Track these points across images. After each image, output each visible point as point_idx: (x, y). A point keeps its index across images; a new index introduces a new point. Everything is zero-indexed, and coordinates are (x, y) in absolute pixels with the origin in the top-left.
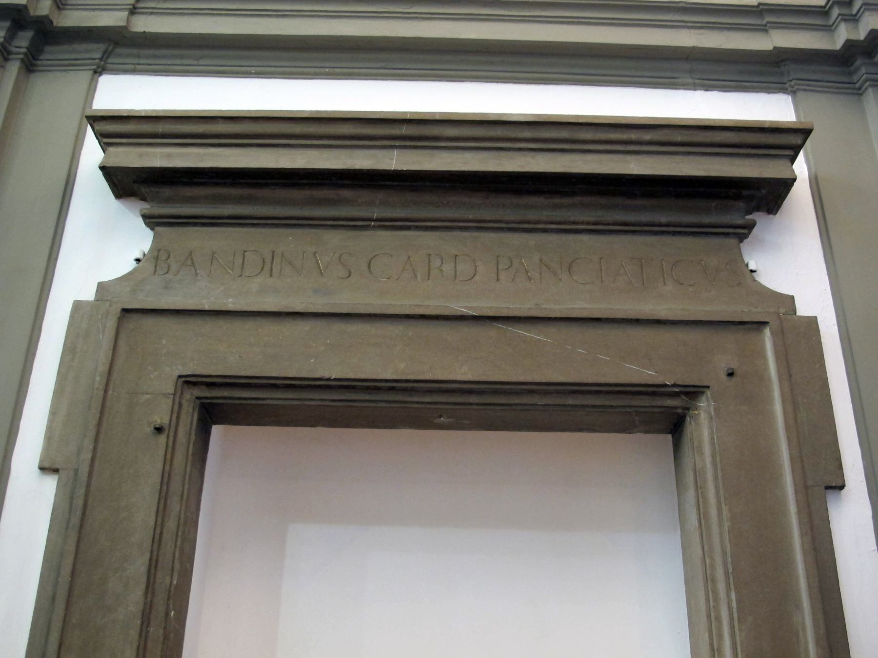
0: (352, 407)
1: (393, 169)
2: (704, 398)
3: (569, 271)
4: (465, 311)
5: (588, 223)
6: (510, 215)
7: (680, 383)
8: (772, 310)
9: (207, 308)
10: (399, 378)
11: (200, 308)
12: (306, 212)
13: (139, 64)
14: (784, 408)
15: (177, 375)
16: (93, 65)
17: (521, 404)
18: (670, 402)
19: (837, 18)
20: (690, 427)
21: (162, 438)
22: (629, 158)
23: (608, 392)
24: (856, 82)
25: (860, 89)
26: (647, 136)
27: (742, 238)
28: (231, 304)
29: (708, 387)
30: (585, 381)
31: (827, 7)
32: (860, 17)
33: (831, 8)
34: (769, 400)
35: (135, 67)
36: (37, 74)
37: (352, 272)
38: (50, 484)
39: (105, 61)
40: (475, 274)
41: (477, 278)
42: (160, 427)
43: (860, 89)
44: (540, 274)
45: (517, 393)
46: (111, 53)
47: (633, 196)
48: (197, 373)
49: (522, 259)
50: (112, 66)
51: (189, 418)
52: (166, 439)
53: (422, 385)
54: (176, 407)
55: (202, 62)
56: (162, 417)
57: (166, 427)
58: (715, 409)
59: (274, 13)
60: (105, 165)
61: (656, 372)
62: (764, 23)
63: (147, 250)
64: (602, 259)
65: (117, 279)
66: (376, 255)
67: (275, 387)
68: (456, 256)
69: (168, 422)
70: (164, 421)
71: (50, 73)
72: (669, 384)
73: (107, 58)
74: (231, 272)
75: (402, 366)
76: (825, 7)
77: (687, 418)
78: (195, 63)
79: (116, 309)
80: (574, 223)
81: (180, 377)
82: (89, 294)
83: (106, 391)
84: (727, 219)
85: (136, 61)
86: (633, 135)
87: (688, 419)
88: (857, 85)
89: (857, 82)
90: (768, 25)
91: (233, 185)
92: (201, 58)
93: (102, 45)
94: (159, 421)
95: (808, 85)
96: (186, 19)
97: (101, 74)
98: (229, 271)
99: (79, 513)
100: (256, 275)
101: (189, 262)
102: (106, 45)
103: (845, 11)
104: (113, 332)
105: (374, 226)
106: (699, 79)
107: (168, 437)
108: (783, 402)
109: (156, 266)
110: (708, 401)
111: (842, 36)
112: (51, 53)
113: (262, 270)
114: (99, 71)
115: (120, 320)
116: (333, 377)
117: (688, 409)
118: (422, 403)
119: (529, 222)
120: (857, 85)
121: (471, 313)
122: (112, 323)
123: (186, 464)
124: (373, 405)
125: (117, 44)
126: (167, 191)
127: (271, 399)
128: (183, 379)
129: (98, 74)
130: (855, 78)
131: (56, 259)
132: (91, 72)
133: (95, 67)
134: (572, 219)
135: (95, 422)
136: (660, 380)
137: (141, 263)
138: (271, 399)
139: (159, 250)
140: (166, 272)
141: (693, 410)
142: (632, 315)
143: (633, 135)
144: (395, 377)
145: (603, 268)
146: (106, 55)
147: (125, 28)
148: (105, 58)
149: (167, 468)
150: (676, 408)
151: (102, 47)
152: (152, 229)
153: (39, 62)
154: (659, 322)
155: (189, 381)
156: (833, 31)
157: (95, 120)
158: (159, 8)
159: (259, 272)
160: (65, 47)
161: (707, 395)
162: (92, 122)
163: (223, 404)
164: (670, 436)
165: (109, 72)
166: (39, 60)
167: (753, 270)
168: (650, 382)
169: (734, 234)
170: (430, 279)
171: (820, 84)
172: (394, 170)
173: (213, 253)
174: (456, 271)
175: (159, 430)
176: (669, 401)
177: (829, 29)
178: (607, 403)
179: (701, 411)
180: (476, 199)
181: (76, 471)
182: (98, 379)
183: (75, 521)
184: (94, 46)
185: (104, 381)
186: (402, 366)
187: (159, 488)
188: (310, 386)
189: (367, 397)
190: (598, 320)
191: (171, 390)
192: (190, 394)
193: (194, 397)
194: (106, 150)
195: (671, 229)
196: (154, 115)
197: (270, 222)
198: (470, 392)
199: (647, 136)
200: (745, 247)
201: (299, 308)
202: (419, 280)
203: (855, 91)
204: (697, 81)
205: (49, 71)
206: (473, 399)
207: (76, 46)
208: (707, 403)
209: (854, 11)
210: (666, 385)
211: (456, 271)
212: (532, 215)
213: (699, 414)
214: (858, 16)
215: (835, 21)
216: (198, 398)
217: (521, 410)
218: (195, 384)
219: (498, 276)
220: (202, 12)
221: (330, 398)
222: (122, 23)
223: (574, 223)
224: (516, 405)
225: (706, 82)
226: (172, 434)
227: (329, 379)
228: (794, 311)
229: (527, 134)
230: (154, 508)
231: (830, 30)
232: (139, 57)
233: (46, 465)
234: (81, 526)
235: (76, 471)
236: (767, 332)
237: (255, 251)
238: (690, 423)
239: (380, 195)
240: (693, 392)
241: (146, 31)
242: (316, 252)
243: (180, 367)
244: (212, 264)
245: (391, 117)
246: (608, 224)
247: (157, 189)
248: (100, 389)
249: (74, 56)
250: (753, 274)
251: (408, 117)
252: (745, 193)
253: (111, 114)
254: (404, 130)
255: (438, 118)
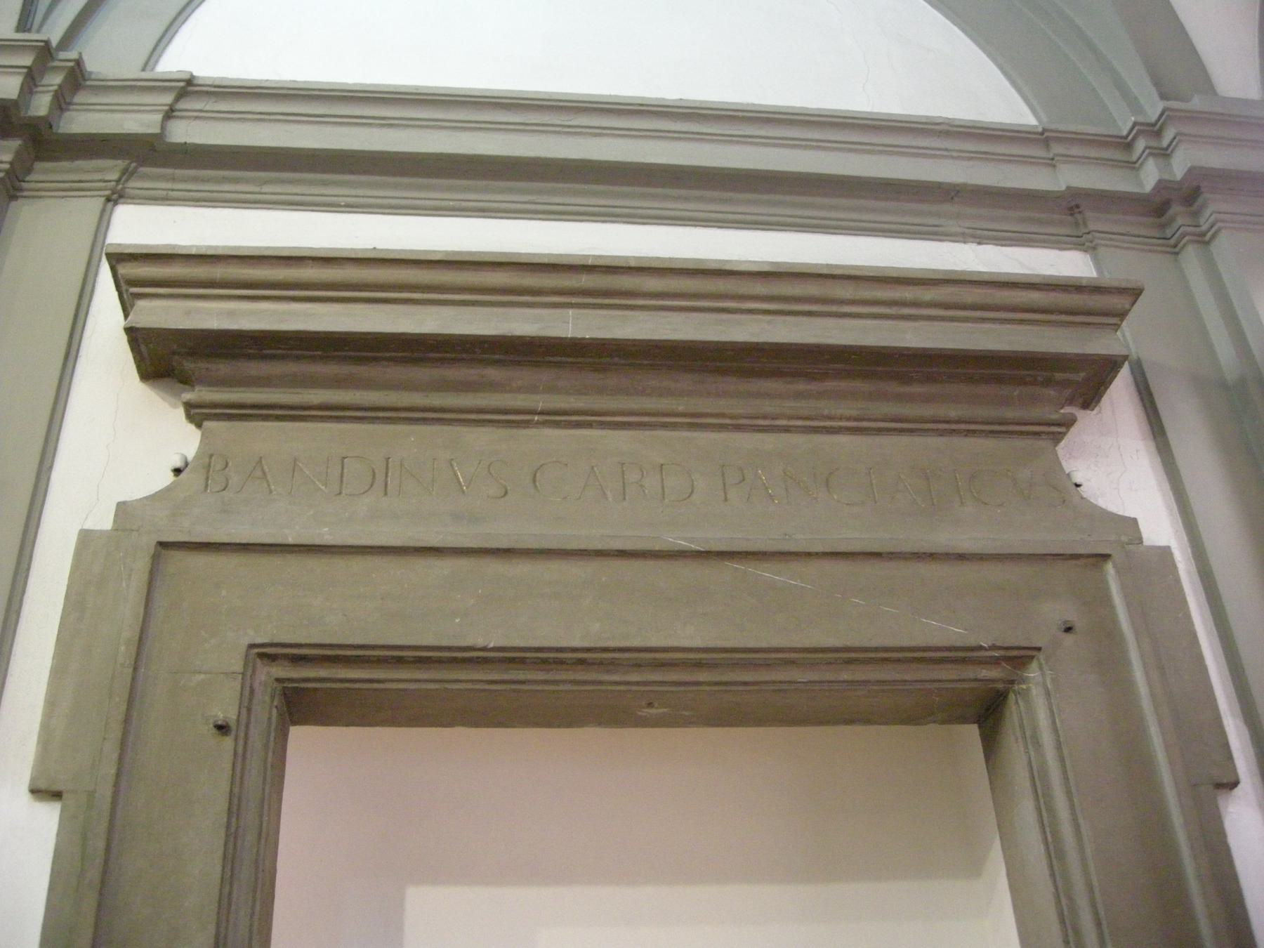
0: (519, 691)
1: (569, 336)
2: (1034, 665)
3: (827, 486)
4: (684, 544)
5: (849, 419)
6: (738, 407)
7: (999, 644)
8: (1113, 537)
9: (291, 541)
10: (592, 645)
11: (279, 540)
12: (437, 400)
13: (173, 190)
14: (1147, 673)
15: (247, 644)
16: (106, 190)
17: (774, 682)
18: (985, 673)
19: (1144, 152)
20: (1014, 710)
21: (228, 742)
22: (902, 324)
23: (898, 660)
24: (1169, 237)
25: (1175, 246)
26: (928, 294)
27: (1057, 438)
28: (326, 536)
29: (1039, 649)
30: (866, 644)
31: (1130, 138)
32: (1172, 152)
33: (1134, 139)
34: (1127, 663)
35: (167, 194)
36: (20, 201)
37: (509, 488)
38: (48, 817)
39: (123, 184)
40: (692, 492)
41: (694, 497)
42: (224, 723)
43: (1175, 246)
44: (786, 489)
45: (767, 665)
46: (132, 174)
47: (904, 379)
48: (276, 640)
49: (757, 470)
50: (131, 192)
51: (266, 709)
52: (233, 744)
53: (627, 655)
54: (247, 692)
55: (266, 189)
56: (226, 710)
57: (233, 724)
58: (1053, 680)
59: (377, 122)
60: (134, 325)
61: (966, 630)
62: (1051, 156)
63: (190, 456)
64: (871, 469)
65: (146, 498)
66: (544, 464)
67: (400, 661)
68: (662, 465)
69: (235, 717)
70: (229, 716)
71: (42, 200)
72: (985, 645)
73: (127, 180)
74: (323, 488)
75: (596, 627)
76: (1154, 125)
77: (1010, 696)
78: (257, 189)
79: (148, 542)
80: (830, 418)
81: (252, 646)
82: (104, 521)
83: (135, 669)
84: (1037, 412)
85: (169, 185)
86: (907, 293)
87: (1012, 697)
88: (1172, 242)
89: (1172, 237)
90: (1056, 158)
91: (325, 358)
92: (266, 182)
93: (119, 162)
94: (221, 716)
95: (1111, 239)
96: (248, 127)
97: (116, 203)
98: (320, 486)
99: (99, 861)
100: (364, 493)
101: (258, 473)
102: (127, 162)
103: (1153, 143)
104: (145, 577)
105: (538, 423)
106: (969, 228)
107: (236, 740)
108: (1145, 666)
109: (207, 479)
110: (1041, 668)
111: (1149, 177)
112: (44, 172)
113: (372, 486)
114: (116, 197)
115: (156, 558)
116: (492, 645)
117: (1012, 682)
118: (628, 683)
119: (765, 417)
120: (1172, 242)
121: (694, 547)
122: (142, 564)
123: (264, 783)
124: (552, 688)
125: (143, 161)
126: (223, 368)
127: (392, 681)
128: (256, 650)
129: (112, 203)
130: (1169, 233)
131: (51, 468)
132: (103, 199)
133: (107, 193)
134: (826, 412)
135: (121, 717)
136: (972, 641)
137: (183, 476)
138: (392, 681)
139: (211, 456)
140: (223, 488)
141: (1018, 684)
142: (926, 547)
143: (907, 293)
144: (586, 644)
145: (874, 482)
146: (127, 174)
147: (160, 136)
148: (123, 179)
149: (236, 790)
150: (993, 681)
151: (121, 164)
152: (199, 426)
153: (25, 185)
154: (962, 557)
155: (266, 654)
156: (1138, 169)
157: (118, 259)
158: (207, 111)
159: (367, 488)
160: (65, 164)
161: (1038, 659)
162: (114, 263)
163: (316, 689)
164: (972, 732)
165: (129, 201)
166: (24, 181)
167: (1078, 483)
168: (958, 644)
169: (1048, 433)
170: (627, 498)
171: (1126, 238)
172: (571, 339)
173: (295, 460)
174: (663, 488)
175: (222, 728)
176: (984, 671)
177: (1133, 166)
178: (898, 677)
179: (1031, 685)
180: (686, 381)
181: (91, 794)
182: (123, 648)
183: (94, 874)
184: (109, 163)
185: (133, 649)
186: (596, 627)
187: (225, 820)
188: (454, 661)
189: (541, 676)
190: (877, 555)
191: (239, 667)
192: (268, 673)
193: (273, 679)
194: (132, 306)
195: (963, 426)
196: (210, 252)
197: (381, 414)
198: (698, 665)
199: (928, 294)
200: (1061, 448)
201: (434, 541)
202: (610, 499)
203: (1168, 249)
204: (967, 231)
205: (40, 197)
206: (703, 676)
207: (80, 163)
208: (1039, 673)
209: (1165, 143)
210: (981, 648)
211: (663, 488)
212: (769, 406)
213: (1028, 689)
214: (1170, 150)
215: (1141, 155)
216: (278, 680)
217: (774, 691)
218: (272, 658)
219: (725, 494)
220: (272, 117)
221: (485, 678)
222: (156, 130)
223: (830, 418)
224: (766, 682)
225: (979, 232)
226: (242, 735)
227: (484, 649)
228: (1140, 540)
229: (760, 288)
230: (220, 853)
231: (1134, 168)
232: (174, 179)
233: (42, 785)
234: (103, 882)
235: (91, 794)
236: (1109, 568)
237: (358, 457)
238: (1017, 702)
239: (545, 376)
240: (1019, 658)
241: (188, 142)
242: (452, 460)
243: (251, 632)
244: (293, 477)
245: (564, 262)
246: (875, 420)
247: (207, 365)
248: (126, 665)
249: (76, 177)
250: (1078, 489)
251: (590, 262)
252: (1059, 376)
253: (145, 251)
254: (585, 281)
255: (633, 264)
